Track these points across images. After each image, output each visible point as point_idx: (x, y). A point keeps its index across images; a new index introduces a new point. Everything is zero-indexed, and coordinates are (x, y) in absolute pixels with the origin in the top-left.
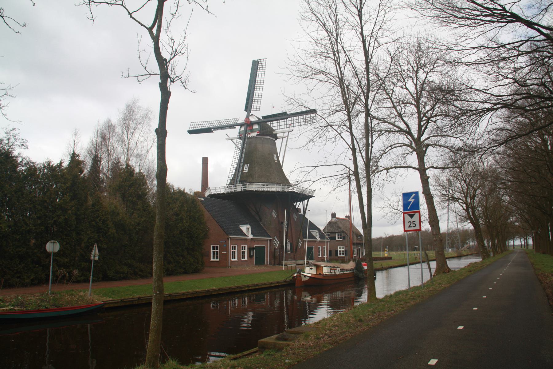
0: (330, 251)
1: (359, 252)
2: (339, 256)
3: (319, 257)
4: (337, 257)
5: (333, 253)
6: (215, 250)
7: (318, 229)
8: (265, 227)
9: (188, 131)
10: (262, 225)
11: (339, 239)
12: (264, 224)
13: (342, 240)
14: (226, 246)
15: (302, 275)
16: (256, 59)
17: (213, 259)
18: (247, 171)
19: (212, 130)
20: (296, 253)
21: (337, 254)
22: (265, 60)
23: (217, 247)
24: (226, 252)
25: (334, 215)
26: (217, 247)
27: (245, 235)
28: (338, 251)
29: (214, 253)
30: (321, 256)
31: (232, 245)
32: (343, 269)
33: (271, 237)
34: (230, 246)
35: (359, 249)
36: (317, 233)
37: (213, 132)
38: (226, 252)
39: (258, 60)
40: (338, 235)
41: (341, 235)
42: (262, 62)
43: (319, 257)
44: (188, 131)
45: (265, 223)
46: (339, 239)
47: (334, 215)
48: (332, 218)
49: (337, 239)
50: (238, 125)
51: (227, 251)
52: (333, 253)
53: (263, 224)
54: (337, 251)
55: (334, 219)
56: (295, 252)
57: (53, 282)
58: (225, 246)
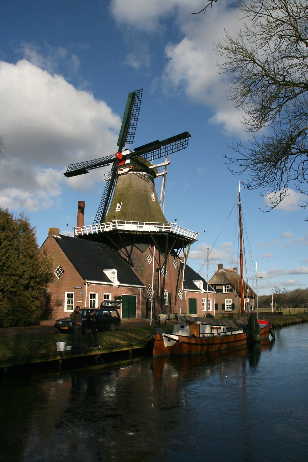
0: (216, 305)
1: (248, 306)
2: (226, 310)
3: (203, 310)
4: (223, 312)
5: (220, 307)
6: (70, 299)
7: (203, 280)
8: (138, 273)
9: (64, 174)
10: (134, 271)
11: (226, 292)
12: (136, 270)
13: (229, 293)
14: (83, 293)
15: (164, 338)
16: (132, 91)
17: (67, 309)
18: (119, 210)
19: (87, 170)
20: (175, 305)
21: (223, 308)
22: (141, 91)
23: (72, 294)
24: (81, 301)
25: (220, 266)
26: (72, 294)
27: (110, 281)
28: (224, 304)
29: (68, 302)
30: (205, 310)
31: (90, 293)
32: (231, 328)
33: (144, 285)
34: (88, 293)
35: (248, 303)
36: (201, 283)
37: (88, 173)
38: (81, 301)
39: (134, 92)
40: (225, 288)
41: (228, 287)
42: (139, 93)
43: (203, 310)
44: (64, 174)
45: (138, 269)
46: (226, 292)
47: (220, 266)
48: (218, 269)
49: (224, 291)
50: (110, 161)
51: (83, 299)
52: (220, 307)
53: (135, 270)
54: (223, 305)
55: (221, 270)
56: (174, 305)
57: (259, 308)
58: (81, 293)
